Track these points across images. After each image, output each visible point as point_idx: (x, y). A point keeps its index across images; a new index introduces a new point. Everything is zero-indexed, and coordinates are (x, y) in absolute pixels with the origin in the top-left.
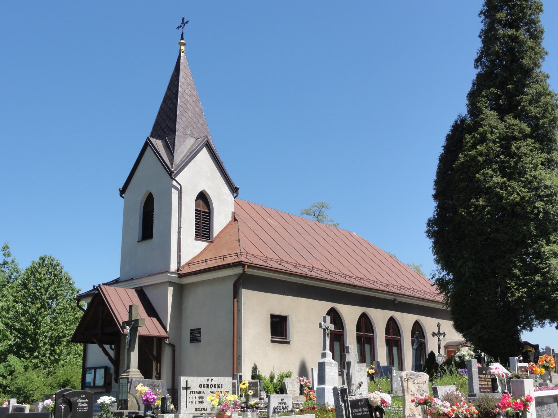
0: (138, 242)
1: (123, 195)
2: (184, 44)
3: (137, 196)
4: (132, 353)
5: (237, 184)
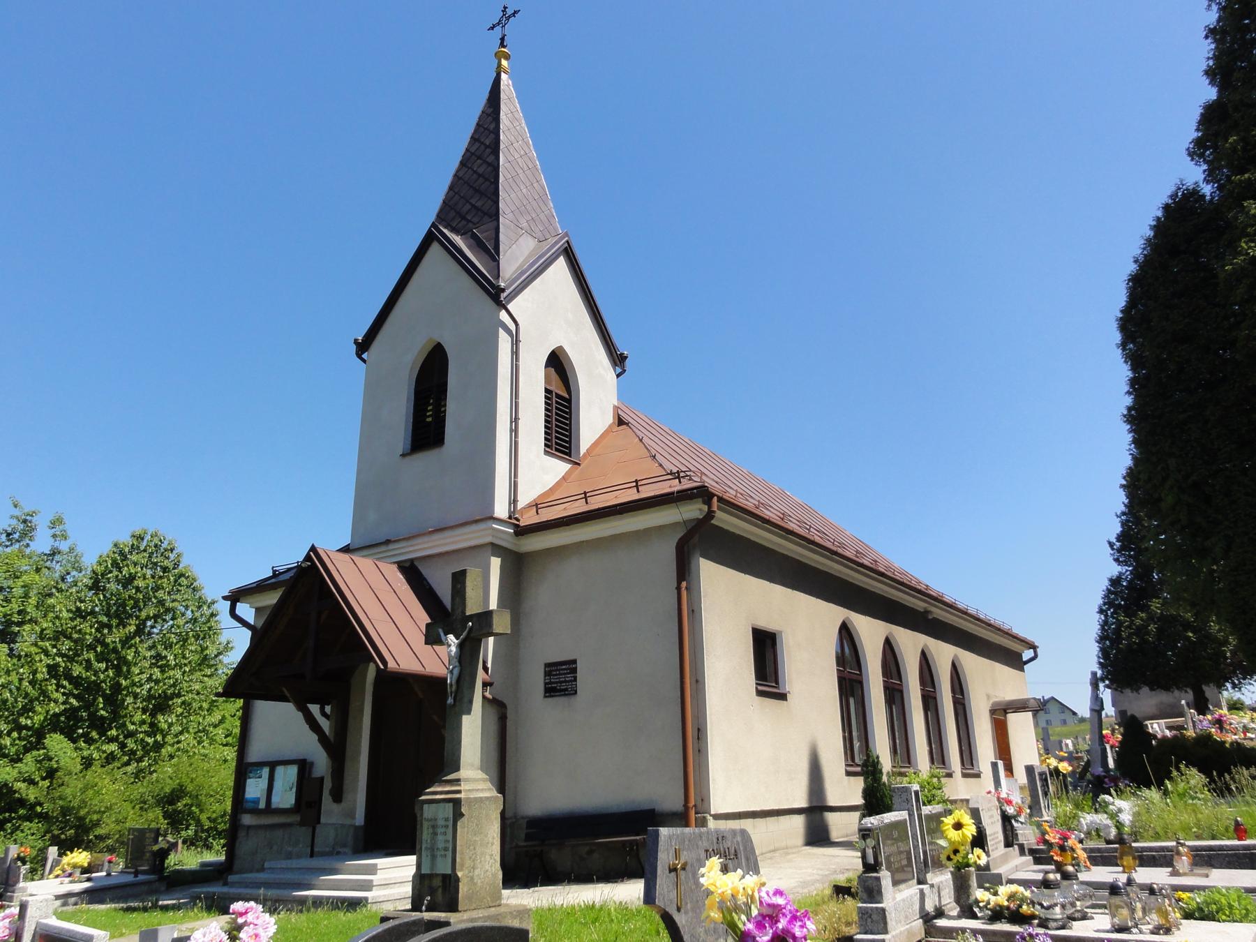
0: (403, 455)
1: (365, 356)
2: (507, 57)
3: (401, 354)
4: (465, 718)
5: (622, 349)
